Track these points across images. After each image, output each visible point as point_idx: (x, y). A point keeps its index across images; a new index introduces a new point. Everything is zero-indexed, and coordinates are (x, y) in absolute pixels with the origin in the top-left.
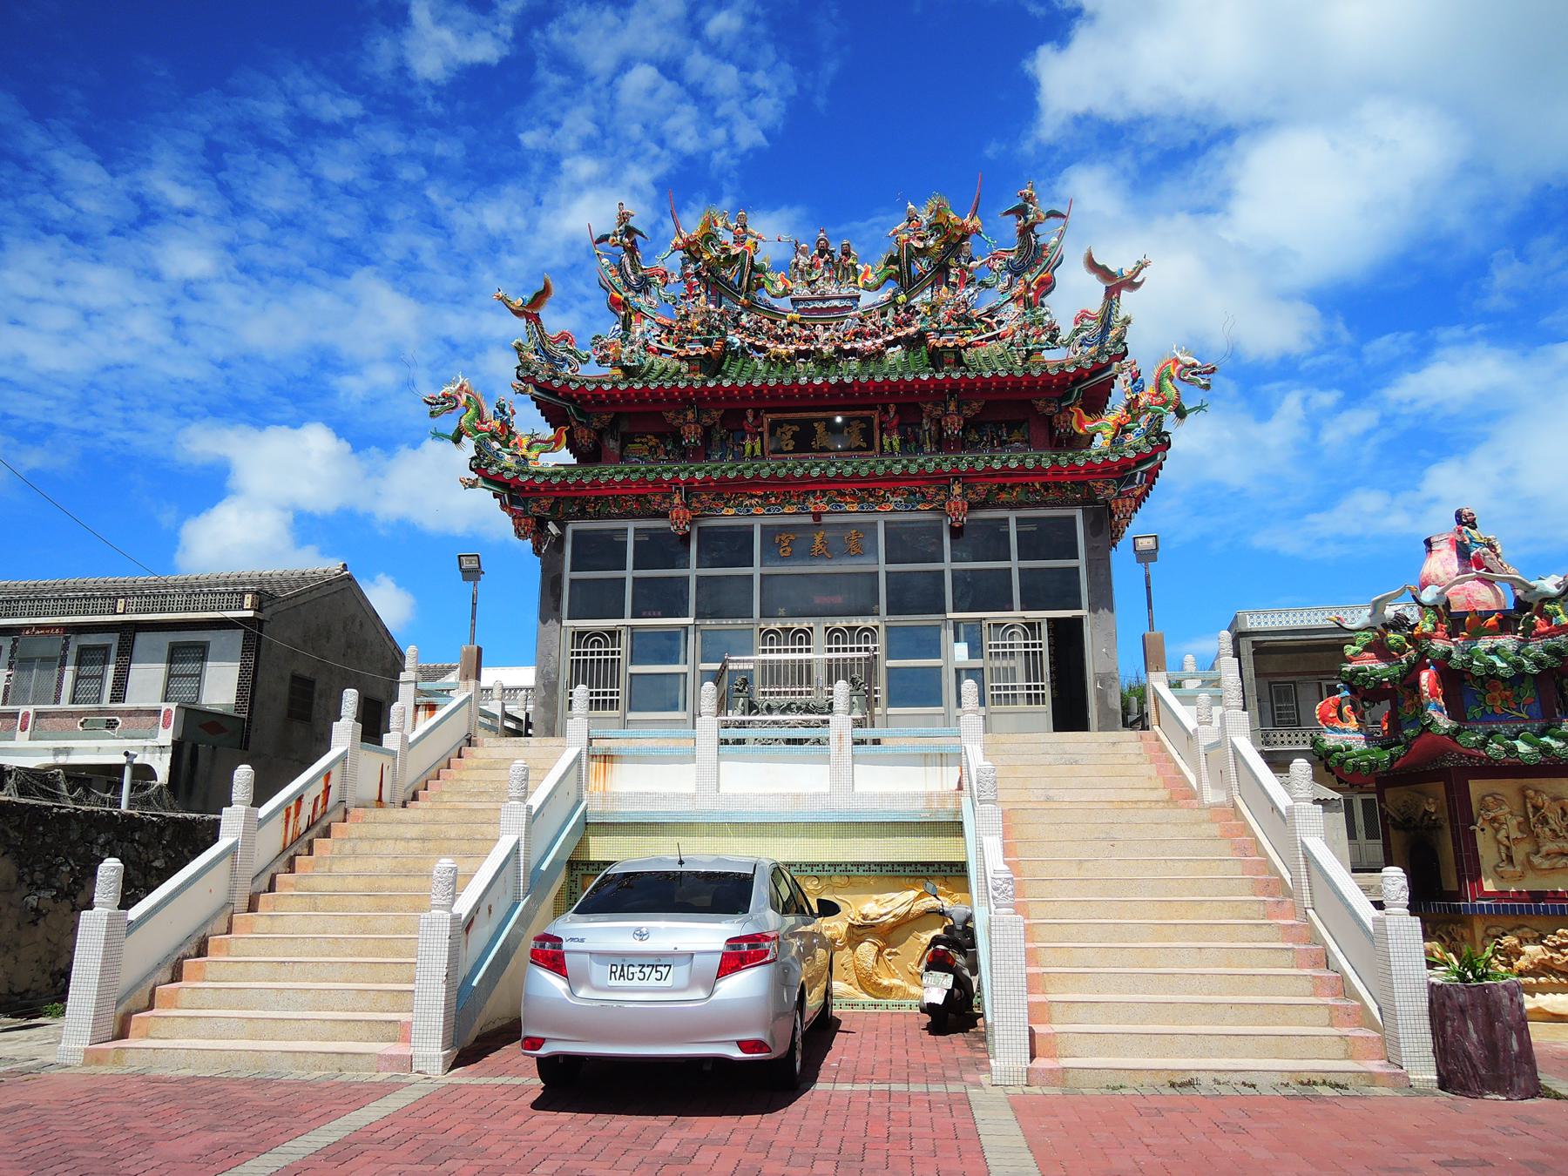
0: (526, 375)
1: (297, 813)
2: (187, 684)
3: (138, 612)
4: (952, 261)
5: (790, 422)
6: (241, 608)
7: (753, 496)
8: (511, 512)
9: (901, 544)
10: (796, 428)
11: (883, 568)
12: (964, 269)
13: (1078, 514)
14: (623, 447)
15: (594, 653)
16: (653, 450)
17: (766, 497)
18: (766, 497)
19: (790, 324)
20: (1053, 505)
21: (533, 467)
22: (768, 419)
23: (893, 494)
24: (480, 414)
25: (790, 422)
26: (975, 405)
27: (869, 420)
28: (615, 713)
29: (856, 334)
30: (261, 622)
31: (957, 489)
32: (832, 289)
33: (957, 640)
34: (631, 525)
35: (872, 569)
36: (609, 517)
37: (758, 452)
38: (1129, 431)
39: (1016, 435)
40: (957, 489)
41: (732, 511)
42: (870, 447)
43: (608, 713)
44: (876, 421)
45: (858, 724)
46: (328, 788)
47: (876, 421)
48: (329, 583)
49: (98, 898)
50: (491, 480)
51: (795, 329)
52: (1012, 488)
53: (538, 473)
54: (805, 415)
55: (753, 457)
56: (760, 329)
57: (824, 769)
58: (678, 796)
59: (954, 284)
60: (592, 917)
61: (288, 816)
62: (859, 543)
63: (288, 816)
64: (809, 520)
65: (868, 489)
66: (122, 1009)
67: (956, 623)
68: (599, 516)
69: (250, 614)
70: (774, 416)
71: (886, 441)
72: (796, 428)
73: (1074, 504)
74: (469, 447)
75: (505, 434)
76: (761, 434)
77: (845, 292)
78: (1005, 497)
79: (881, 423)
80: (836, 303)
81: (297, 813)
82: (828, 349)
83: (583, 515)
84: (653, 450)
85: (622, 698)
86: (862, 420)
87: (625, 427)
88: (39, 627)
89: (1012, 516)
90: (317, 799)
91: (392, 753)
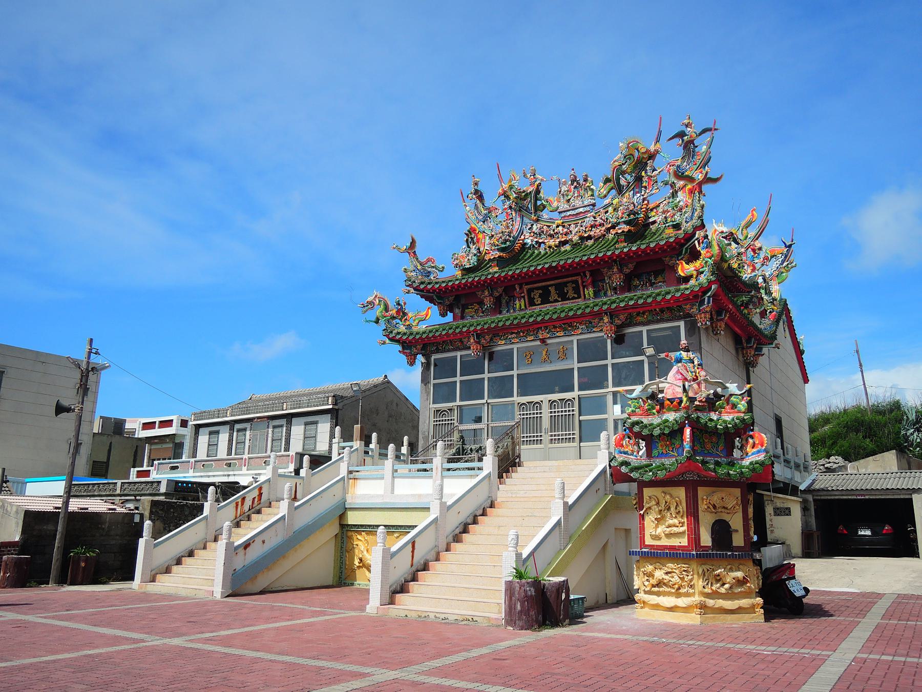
0: (410, 283)
1: (242, 504)
2: (312, 441)
3: (291, 409)
4: (643, 174)
5: (537, 289)
6: (328, 404)
7: (512, 333)
8: (404, 353)
9: (589, 351)
10: (540, 291)
11: (576, 365)
12: (650, 177)
13: (682, 324)
14: (463, 312)
15: (560, 410)
16: (476, 311)
17: (518, 333)
18: (518, 333)
19: (558, 226)
20: (668, 320)
21: (415, 329)
22: (525, 288)
23: (580, 324)
24: (387, 309)
25: (537, 289)
26: (630, 266)
27: (576, 282)
28: (542, 446)
29: (592, 226)
30: (337, 410)
31: (606, 319)
32: (578, 203)
33: (615, 403)
34: (459, 354)
35: (571, 367)
36: (449, 351)
37: (523, 307)
38: (702, 273)
39: (660, 278)
40: (606, 319)
41: (503, 342)
42: (579, 297)
43: (535, 446)
44: (580, 282)
45: (450, 461)
46: (260, 495)
47: (580, 282)
48: (376, 386)
49: (144, 534)
50: (393, 340)
51: (560, 228)
52: (644, 313)
53: (417, 333)
54: (544, 284)
55: (521, 310)
56: (543, 232)
57: (430, 481)
58: (378, 496)
59: (645, 187)
60: (863, 595)
61: (237, 505)
62: (564, 354)
63: (237, 505)
64: (538, 343)
65: (567, 324)
66: (153, 572)
67: (615, 394)
68: (444, 351)
69: (331, 407)
70: (529, 287)
71: (586, 292)
72: (540, 291)
73: (679, 318)
74: (383, 325)
75: (402, 313)
76: (524, 297)
77: (586, 203)
78: (640, 319)
79: (583, 282)
80: (581, 210)
81: (242, 504)
82: (576, 239)
83: (438, 351)
84: (476, 311)
85: (577, 437)
86: (573, 282)
87: (463, 302)
88: (259, 418)
89: (644, 329)
90: (254, 499)
91: (303, 478)
